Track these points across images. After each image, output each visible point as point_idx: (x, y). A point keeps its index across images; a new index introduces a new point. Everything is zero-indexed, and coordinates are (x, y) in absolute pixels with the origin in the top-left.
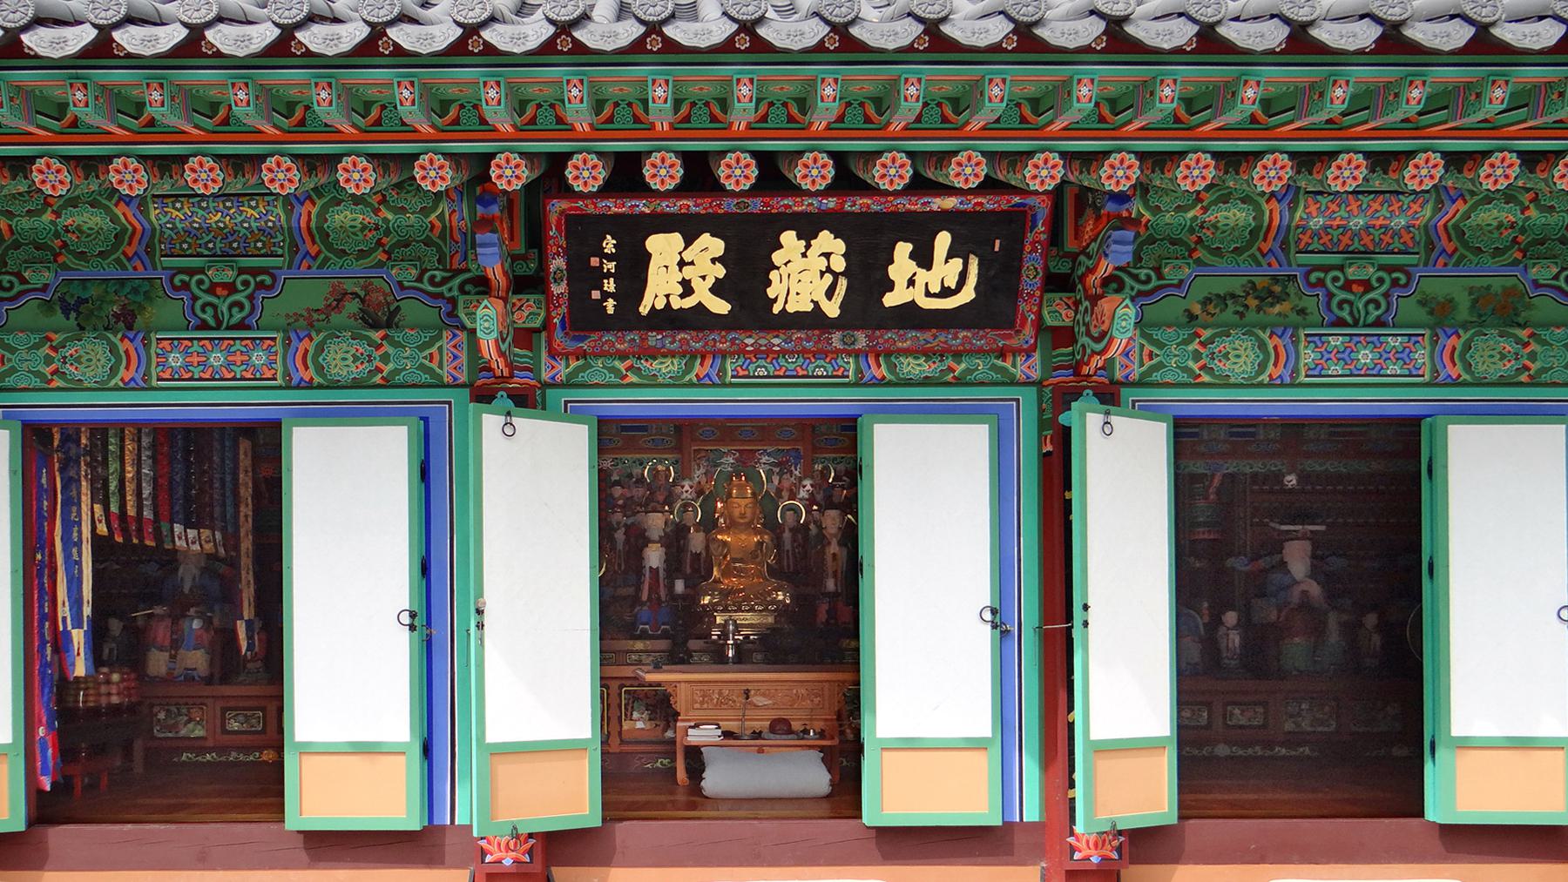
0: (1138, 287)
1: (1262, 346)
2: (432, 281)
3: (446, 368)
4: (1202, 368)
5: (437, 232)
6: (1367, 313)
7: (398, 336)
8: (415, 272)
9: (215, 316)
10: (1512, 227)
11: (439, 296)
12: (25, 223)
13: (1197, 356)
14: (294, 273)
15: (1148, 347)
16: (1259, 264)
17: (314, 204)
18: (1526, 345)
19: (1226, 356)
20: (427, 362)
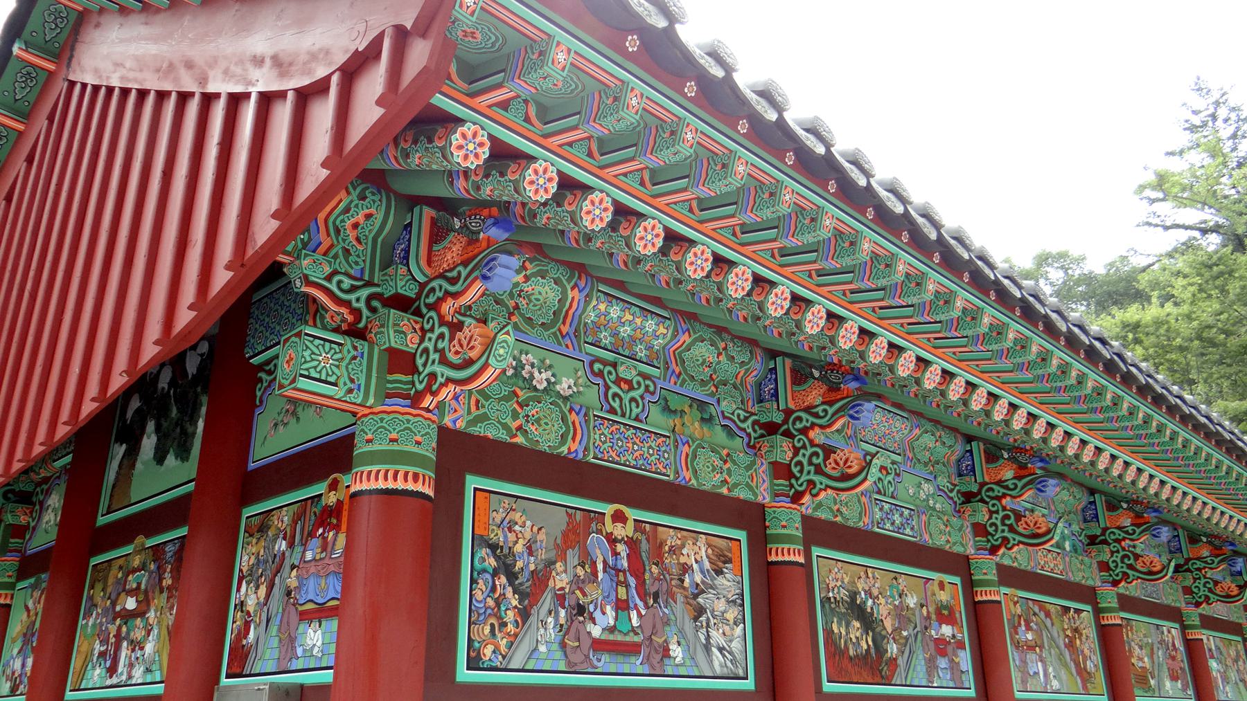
2: (739, 416)
8: (328, 270)
11: (347, 304)
16: (560, 344)
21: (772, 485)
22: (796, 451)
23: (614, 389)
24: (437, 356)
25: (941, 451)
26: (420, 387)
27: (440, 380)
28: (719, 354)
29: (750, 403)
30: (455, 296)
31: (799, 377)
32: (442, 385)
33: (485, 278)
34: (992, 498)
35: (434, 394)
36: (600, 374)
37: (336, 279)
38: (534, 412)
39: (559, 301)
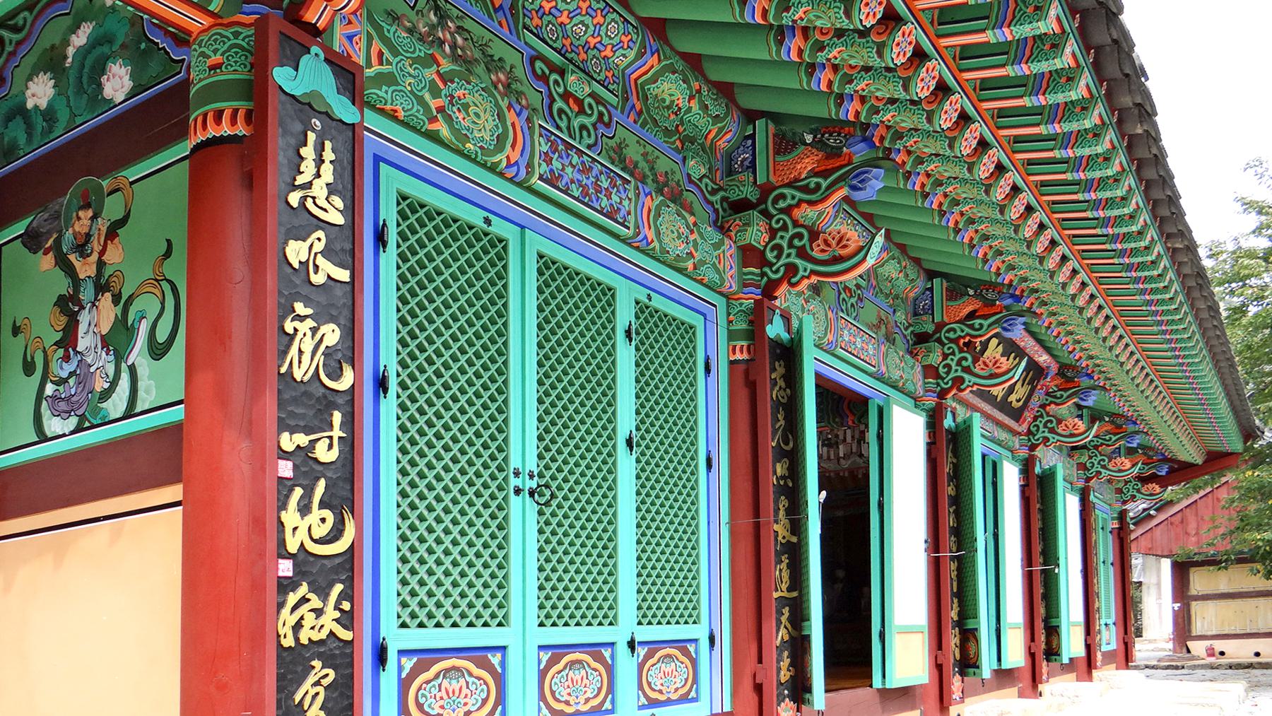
16: (490, 16)
20: (387, 54)
23: (559, 104)
24: (793, 251)
25: (903, 283)
28: (691, 98)
29: (719, 173)
31: (784, 144)
34: (951, 341)
36: (544, 79)
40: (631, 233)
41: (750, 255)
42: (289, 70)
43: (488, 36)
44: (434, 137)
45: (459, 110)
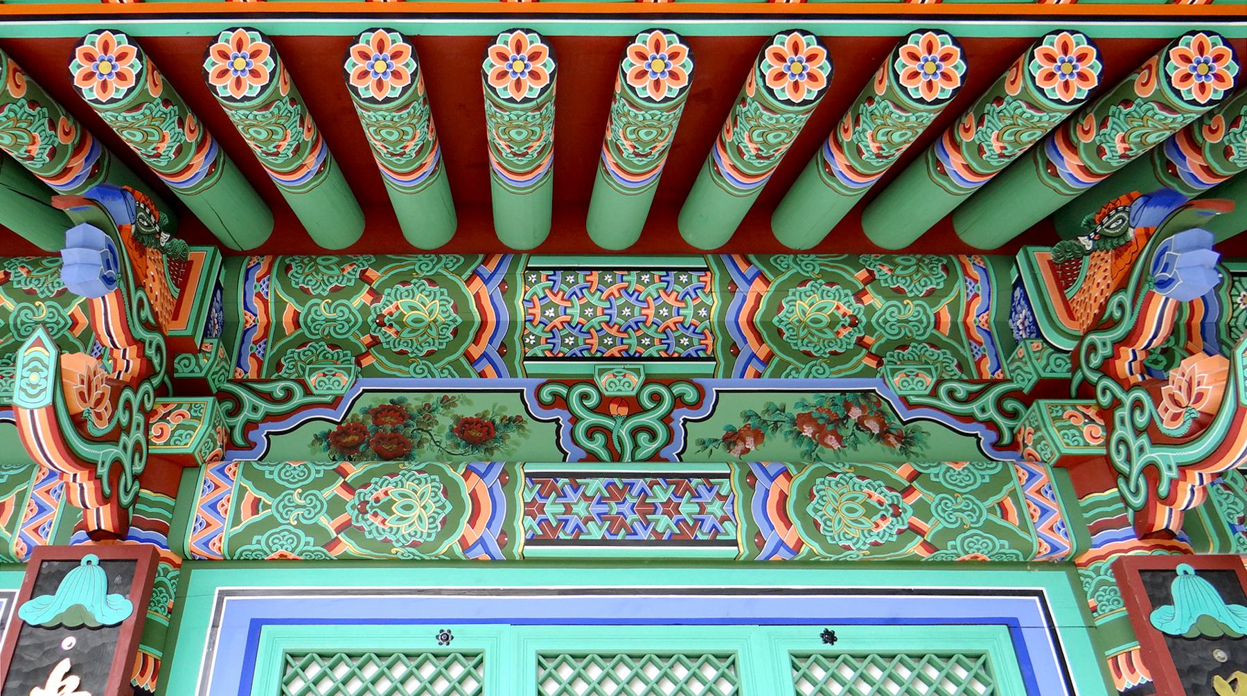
0: (265, 407)
1: (450, 490)
2: (951, 394)
3: (19, 528)
4: (344, 527)
5: (78, 331)
6: (636, 446)
7: (271, 472)
8: (930, 381)
9: (608, 445)
10: (854, 324)
11: (969, 418)
12: (324, 310)
13: (335, 507)
14: (734, 383)
15: (252, 492)
17: (767, 282)
18: (907, 491)
19: (388, 508)
21: (1074, 513)
22: (1107, 414)
24: (1144, 440)
26: (1138, 502)
27: (1166, 475)
30: (1129, 339)
32: (1173, 483)
33: (1163, 284)
35: (1169, 500)
36: (560, 402)
37: (942, 390)
38: (884, 525)
39: (455, 307)
40: (744, 550)
41: (1085, 473)
42: (1165, 608)
43: (395, 396)
44: (347, 561)
45: (881, 504)
